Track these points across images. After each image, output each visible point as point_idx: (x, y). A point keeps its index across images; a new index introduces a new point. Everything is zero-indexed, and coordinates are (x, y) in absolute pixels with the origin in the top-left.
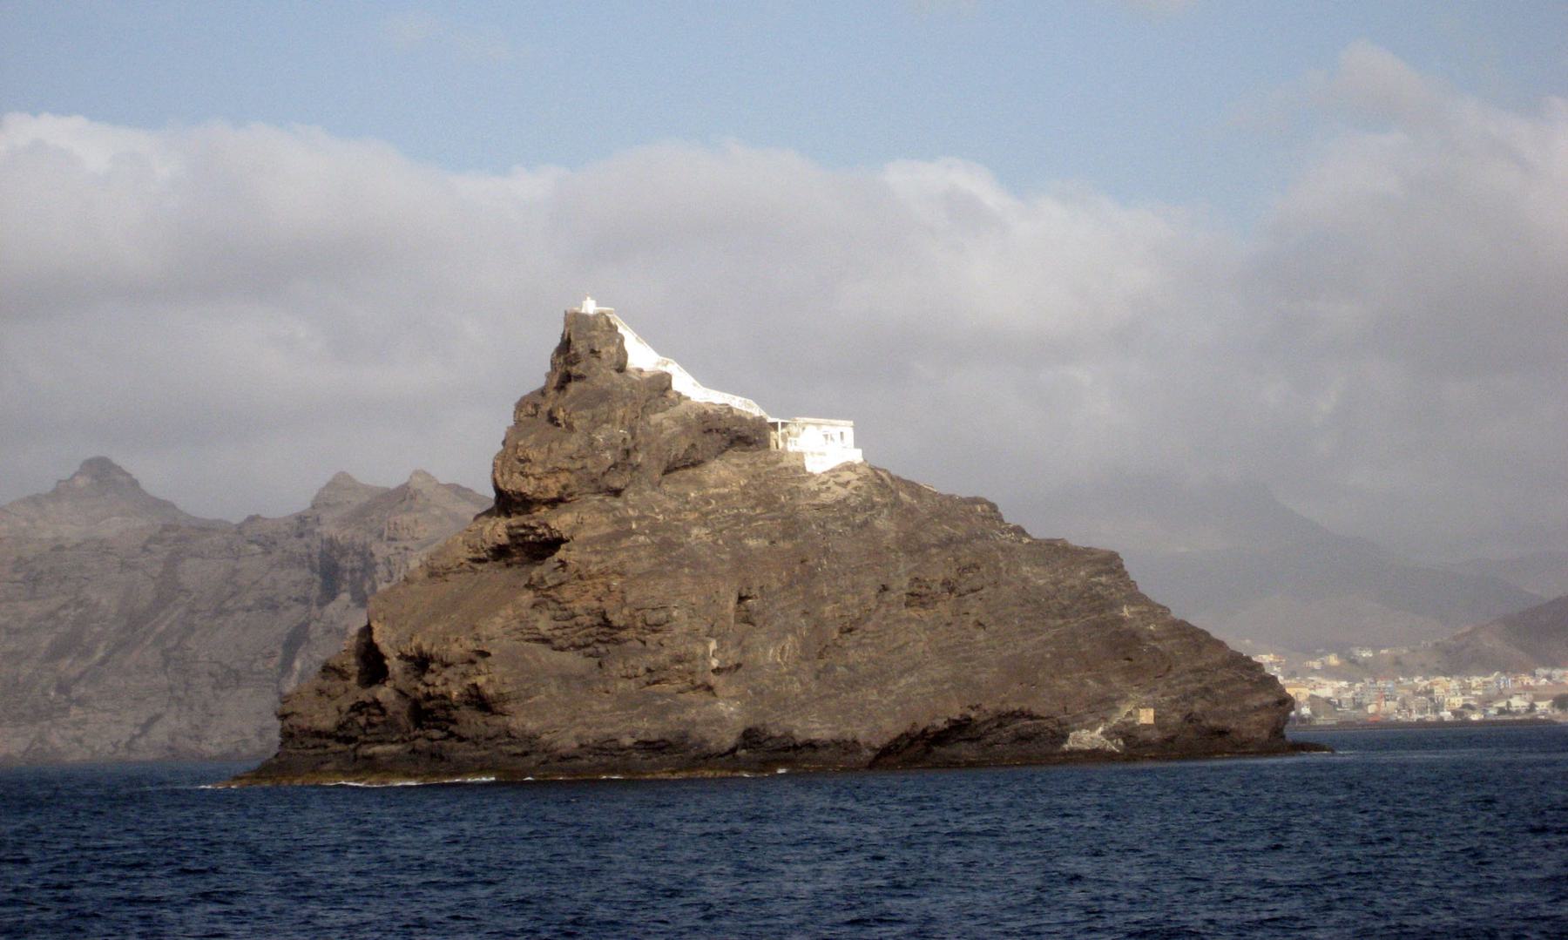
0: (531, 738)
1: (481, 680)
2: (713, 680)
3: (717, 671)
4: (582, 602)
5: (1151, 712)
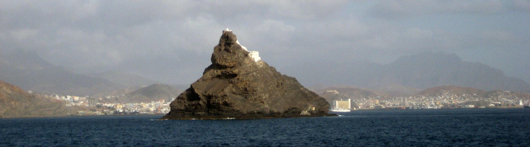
0: (238, 111)
1: (227, 100)
4: (241, 86)
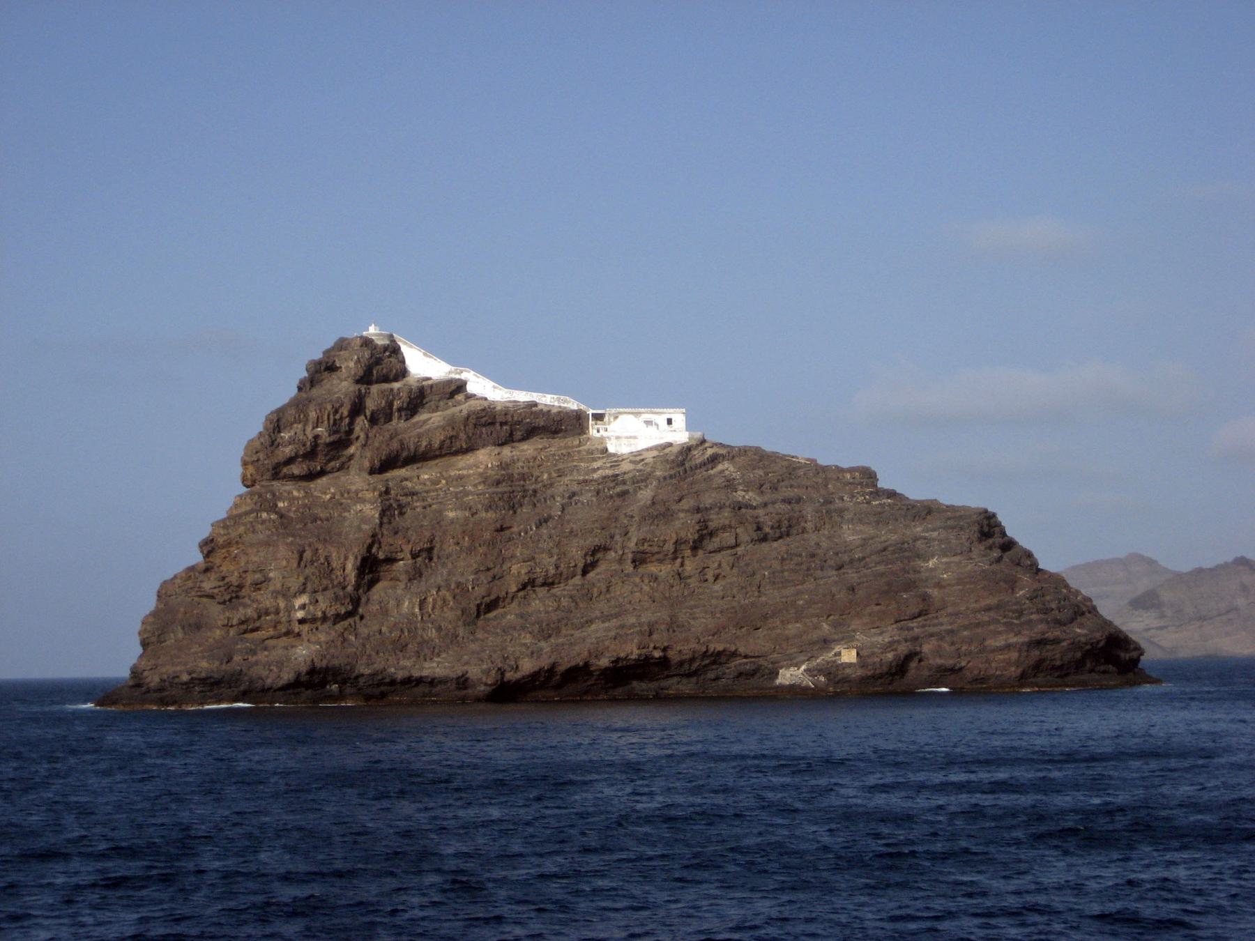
2: (297, 628)
3: (302, 621)
5: (854, 652)
